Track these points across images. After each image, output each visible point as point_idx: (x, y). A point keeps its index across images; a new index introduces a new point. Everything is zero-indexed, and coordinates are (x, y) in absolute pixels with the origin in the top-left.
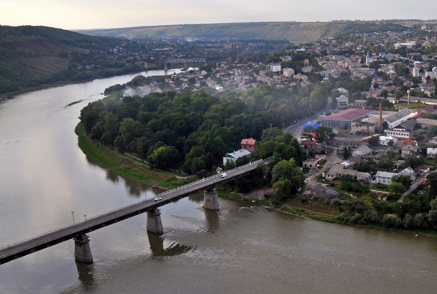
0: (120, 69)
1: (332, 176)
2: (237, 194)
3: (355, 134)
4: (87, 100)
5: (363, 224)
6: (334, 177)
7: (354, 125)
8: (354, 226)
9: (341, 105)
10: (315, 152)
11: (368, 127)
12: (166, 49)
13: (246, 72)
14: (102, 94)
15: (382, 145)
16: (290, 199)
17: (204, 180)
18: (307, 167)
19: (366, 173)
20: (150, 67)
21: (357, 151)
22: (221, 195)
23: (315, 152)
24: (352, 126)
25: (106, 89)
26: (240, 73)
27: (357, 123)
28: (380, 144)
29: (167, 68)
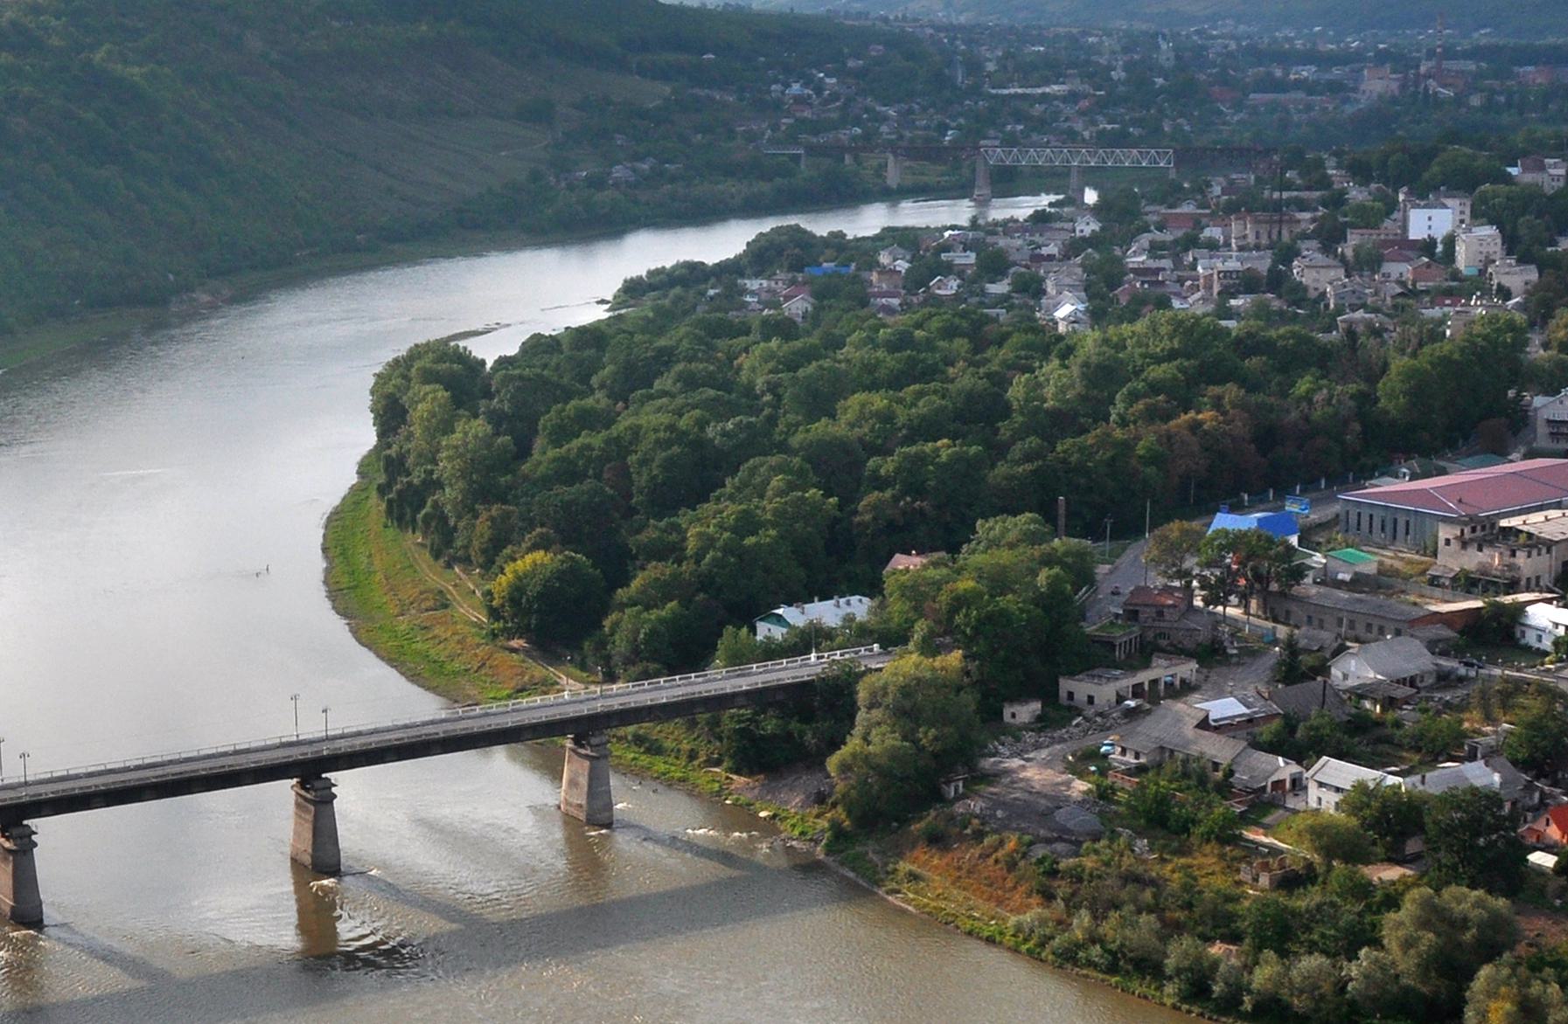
0: (764, 187)
1: (1137, 756)
2: (727, 778)
3: (1447, 583)
4: (522, 327)
5: (1095, 966)
6: (1143, 760)
7: (1451, 537)
8: (1060, 967)
9: (1552, 434)
10: (1171, 645)
11: (1513, 554)
12: (1056, 87)
13: (1280, 233)
14: (603, 302)
15: (1531, 647)
16: (895, 824)
17: (566, 697)
18: (1072, 703)
19: (1280, 759)
20: (910, 180)
21: (1353, 662)
22: (664, 774)
23: (1171, 645)
24: (1441, 543)
25: (625, 281)
26: (1251, 239)
27: (1462, 531)
28: (1523, 642)
29: (987, 191)
